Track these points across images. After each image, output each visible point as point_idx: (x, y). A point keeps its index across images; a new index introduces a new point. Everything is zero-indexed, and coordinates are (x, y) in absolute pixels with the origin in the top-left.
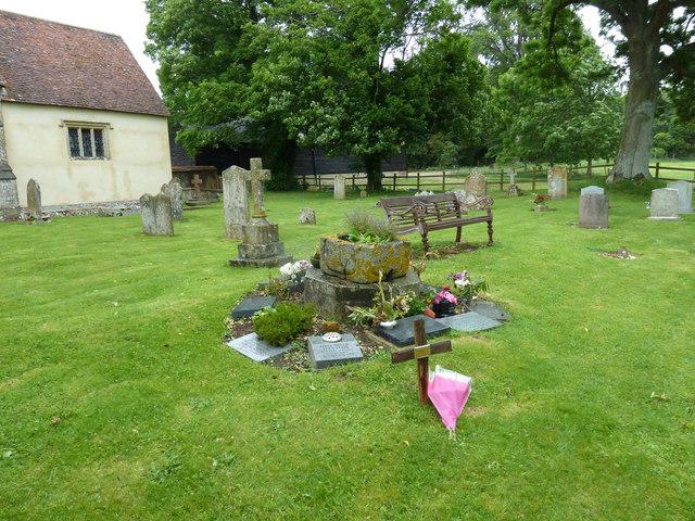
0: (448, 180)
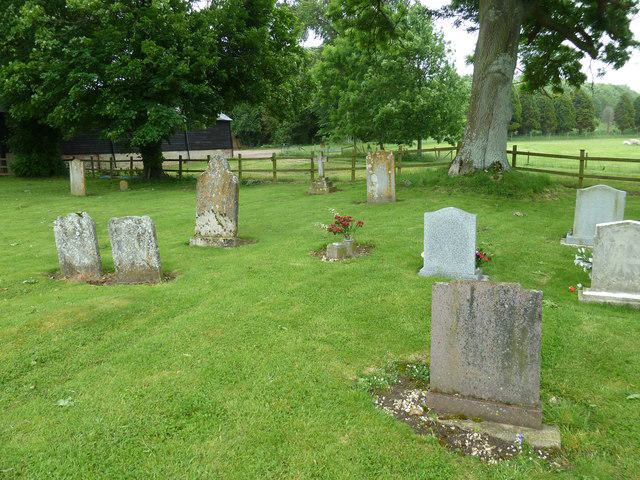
0: (281, 164)
